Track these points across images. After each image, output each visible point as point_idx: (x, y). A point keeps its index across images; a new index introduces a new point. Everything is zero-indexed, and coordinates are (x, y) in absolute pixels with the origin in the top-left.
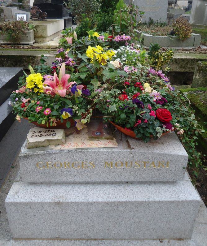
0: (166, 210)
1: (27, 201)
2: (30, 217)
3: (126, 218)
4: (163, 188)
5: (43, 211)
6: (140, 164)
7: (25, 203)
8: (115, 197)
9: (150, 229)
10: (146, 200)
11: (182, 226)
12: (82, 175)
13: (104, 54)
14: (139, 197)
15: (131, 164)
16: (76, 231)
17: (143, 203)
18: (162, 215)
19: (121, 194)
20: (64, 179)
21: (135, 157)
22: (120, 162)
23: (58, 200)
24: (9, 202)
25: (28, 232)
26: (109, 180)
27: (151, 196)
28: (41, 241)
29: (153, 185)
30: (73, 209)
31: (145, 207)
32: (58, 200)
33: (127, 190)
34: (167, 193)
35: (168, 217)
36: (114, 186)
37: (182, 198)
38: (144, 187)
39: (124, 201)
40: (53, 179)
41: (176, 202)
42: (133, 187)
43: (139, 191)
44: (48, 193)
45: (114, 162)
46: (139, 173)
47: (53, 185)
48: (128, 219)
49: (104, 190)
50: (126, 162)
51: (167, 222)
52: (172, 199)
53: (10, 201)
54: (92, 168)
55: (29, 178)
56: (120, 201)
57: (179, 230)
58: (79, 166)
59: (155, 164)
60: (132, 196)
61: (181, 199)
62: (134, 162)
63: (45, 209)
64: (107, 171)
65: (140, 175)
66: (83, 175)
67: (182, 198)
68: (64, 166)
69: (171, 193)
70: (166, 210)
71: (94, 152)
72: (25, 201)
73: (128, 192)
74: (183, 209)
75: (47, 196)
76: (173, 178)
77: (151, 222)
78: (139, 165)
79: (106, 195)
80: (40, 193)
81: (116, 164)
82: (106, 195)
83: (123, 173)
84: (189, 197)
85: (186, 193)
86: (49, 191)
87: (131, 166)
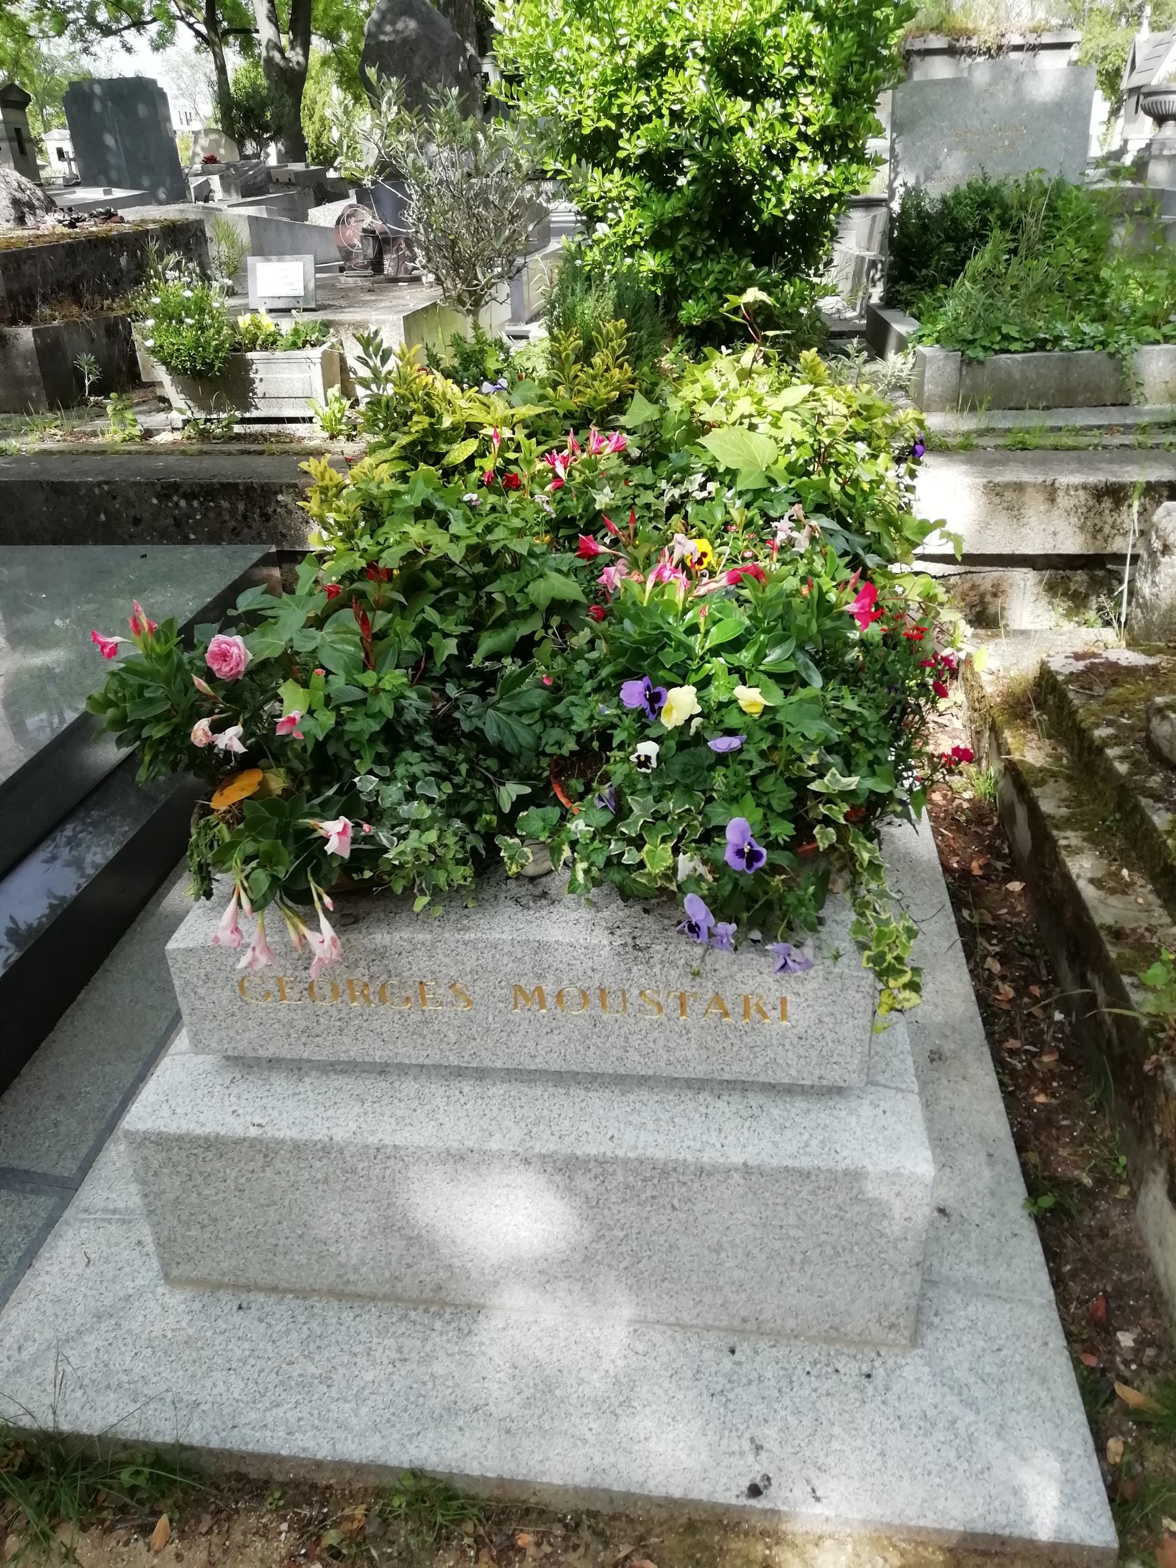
0: (779, 1208)
1: (1101, 907)
2: (220, 1196)
3: (611, 1229)
4: (775, 1112)
5: (269, 1172)
6: (662, 1002)
7: (198, 1137)
8: (557, 1134)
9: (721, 1283)
10: (689, 1158)
11: (865, 1285)
12: (424, 1037)
13: (795, 171)
14: (660, 1141)
15: (625, 1001)
16: (409, 1266)
17: (675, 1169)
18: (765, 1226)
19: (585, 1127)
20: (349, 1049)
21: (635, 969)
22: (573, 991)
23: (325, 1131)
24: (137, 1132)
25: (221, 1257)
26: (538, 1064)
27: (713, 1140)
28: (273, 1298)
29: (736, 1097)
30: (388, 1172)
31: (685, 1184)
32: (325, 1131)
33: (617, 1112)
34: (788, 1133)
35: (796, 1240)
36: (562, 1091)
37: (848, 1161)
38: (691, 1105)
39: (594, 1152)
40: (309, 1048)
41: (822, 1177)
42: (645, 1099)
43: (666, 1116)
44: (291, 1104)
45: (549, 988)
46: (661, 1042)
47: (313, 1073)
48: (622, 1234)
49: (518, 1103)
50: (602, 990)
51: (792, 1260)
52: (804, 1163)
53: (141, 1127)
54: (461, 1006)
55: (216, 1038)
56: (579, 1153)
57: (409, 1266)
58: (408, 999)
59: (729, 1006)
60: (629, 1136)
61: (843, 1166)
62: (636, 992)
63: (279, 1165)
64: (525, 1024)
65: (668, 1050)
66: (429, 1036)
67: (848, 1161)
68: (346, 997)
69: (806, 1136)
70: (779, 1208)
71: (465, 943)
72: (199, 1131)
73: (617, 1117)
74: (856, 1209)
75: (285, 1115)
76: (817, 1073)
77: (723, 1255)
78: (658, 1004)
79: (522, 1124)
80: (259, 1102)
81: (560, 995)
82: (522, 1124)
83: (595, 1039)
84: (883, 1155)
85: (875, 1140)
86: (295, 1094)
87: (625, 1008)
